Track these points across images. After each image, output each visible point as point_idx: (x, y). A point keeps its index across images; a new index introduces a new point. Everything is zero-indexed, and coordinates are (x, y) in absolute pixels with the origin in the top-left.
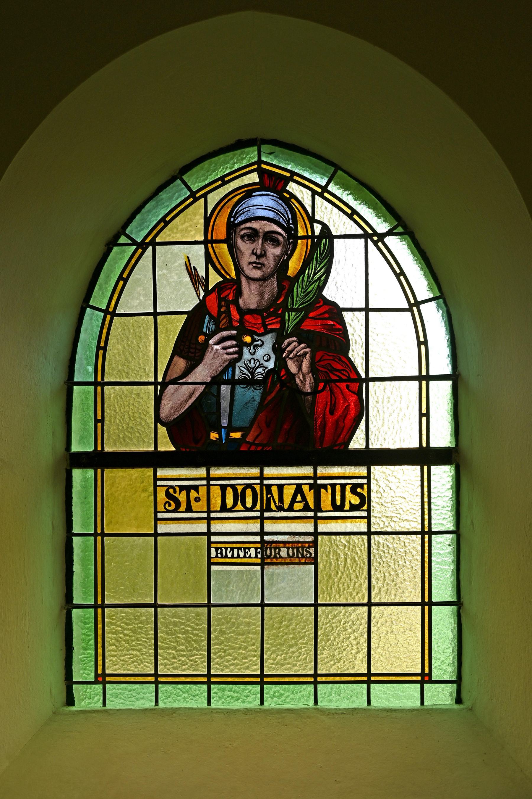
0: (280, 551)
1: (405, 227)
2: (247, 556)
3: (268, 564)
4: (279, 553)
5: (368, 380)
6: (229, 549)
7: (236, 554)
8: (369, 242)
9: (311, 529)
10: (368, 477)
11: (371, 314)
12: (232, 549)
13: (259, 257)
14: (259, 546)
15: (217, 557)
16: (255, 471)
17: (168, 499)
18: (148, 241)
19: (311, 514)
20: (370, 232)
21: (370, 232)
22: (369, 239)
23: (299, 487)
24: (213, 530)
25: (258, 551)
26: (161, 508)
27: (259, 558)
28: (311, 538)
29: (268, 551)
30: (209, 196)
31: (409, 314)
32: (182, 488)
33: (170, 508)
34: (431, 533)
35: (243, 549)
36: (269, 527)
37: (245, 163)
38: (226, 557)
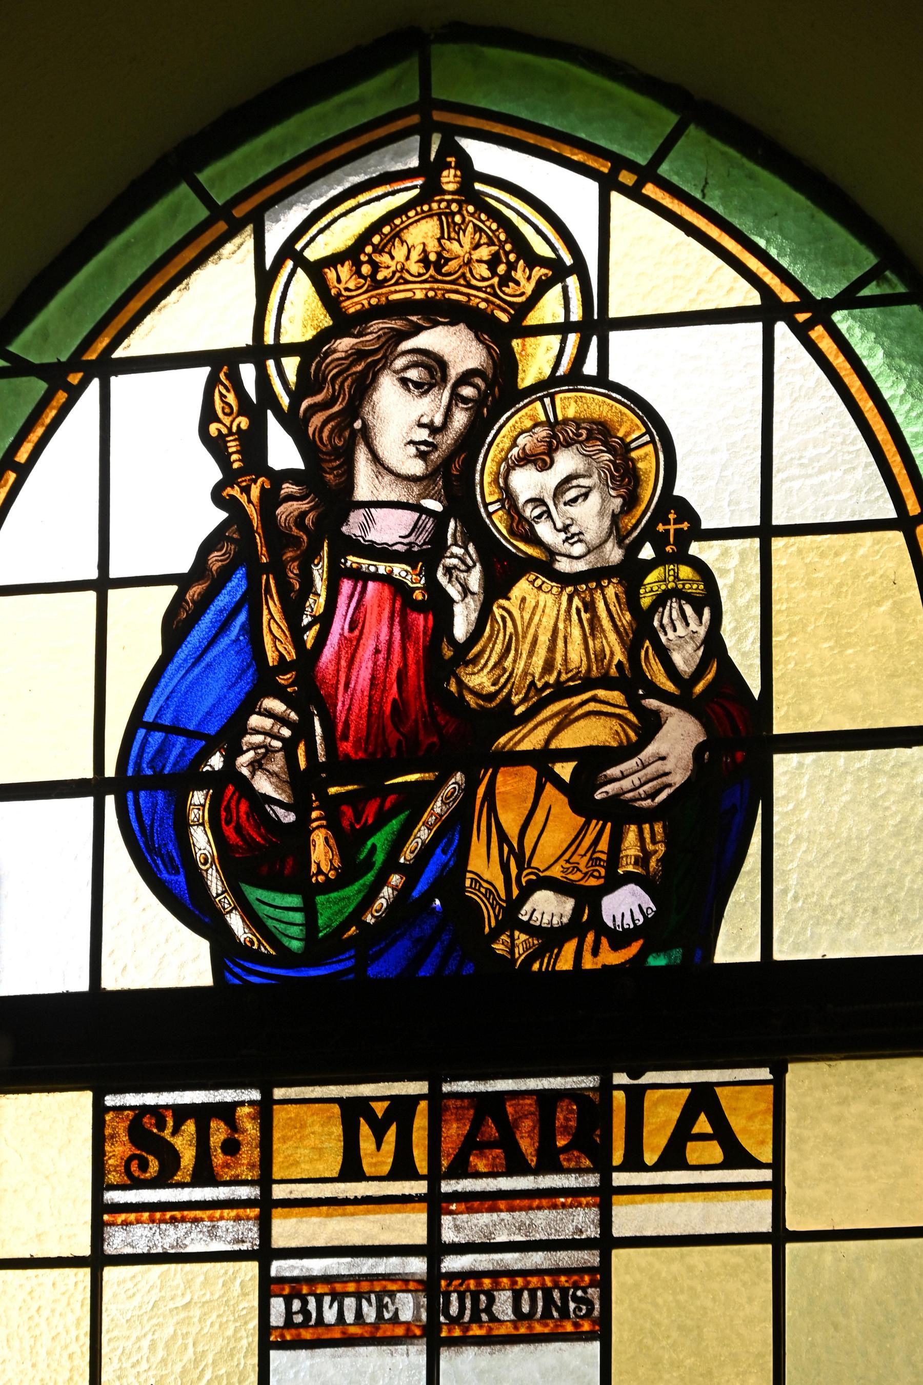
2: (387, 1316)
3: (453, 1342)
4: (488, 1310)
8: (781, 329)
9: (418, 1235)
11: (84, 1275)
13: (434, 430)
15: (289, 1323)
17: (138, 1148)
20: (787, 296)
21: (787, 296)
24: (279, 1241)
27: (421, 1337)
28: (591, 1258)
35: (373, 1297)
37: (796, 271)
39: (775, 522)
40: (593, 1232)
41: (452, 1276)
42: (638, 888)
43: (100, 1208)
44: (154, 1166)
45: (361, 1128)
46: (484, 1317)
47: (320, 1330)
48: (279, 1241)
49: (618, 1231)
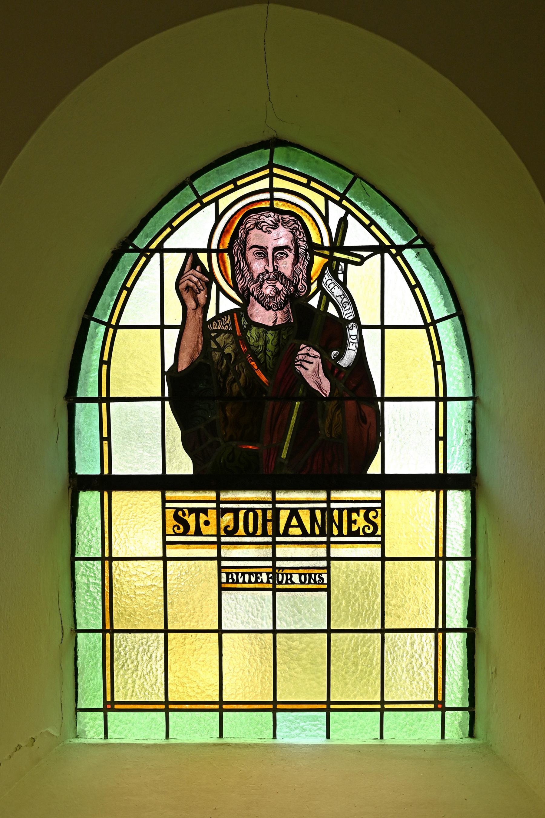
0: (291, 577)
1: (423, 239)
2: (259, 581)
4: (291, 579)
5: (384, 399)
6: (240, 574)
7: (247, 580)
8: (387, 255)
10: (382, 501)
11: (387, 331)
12: (243, 574)
14: (271, 570)
15: (227, 582)
16: (266, 495)
18: (153, 246)
19: (269, 539)
20: (387, 243)
21: (387, 243)
22: (220, 292)
23: (294, 513)
24: (278, 555)
25: (270, 577)
26: (169, 530)
28: (324, 563)
29: (280, 576)
30: (221, 201)
31: (424, 331)
32: (191, 511)
33: (178, 531)
34: (445, 559)
36: (281, 552)
38: (237, 582)
39: (380, 324)
40: (324, 555)
41: (280, 568)
42: (180, 432)
43: (165, 543)
44: (182, 530)
45: (293, 520)
46: (289, 582)
47: (238, 585)
48: (278, 555)
49: (332, 555)
